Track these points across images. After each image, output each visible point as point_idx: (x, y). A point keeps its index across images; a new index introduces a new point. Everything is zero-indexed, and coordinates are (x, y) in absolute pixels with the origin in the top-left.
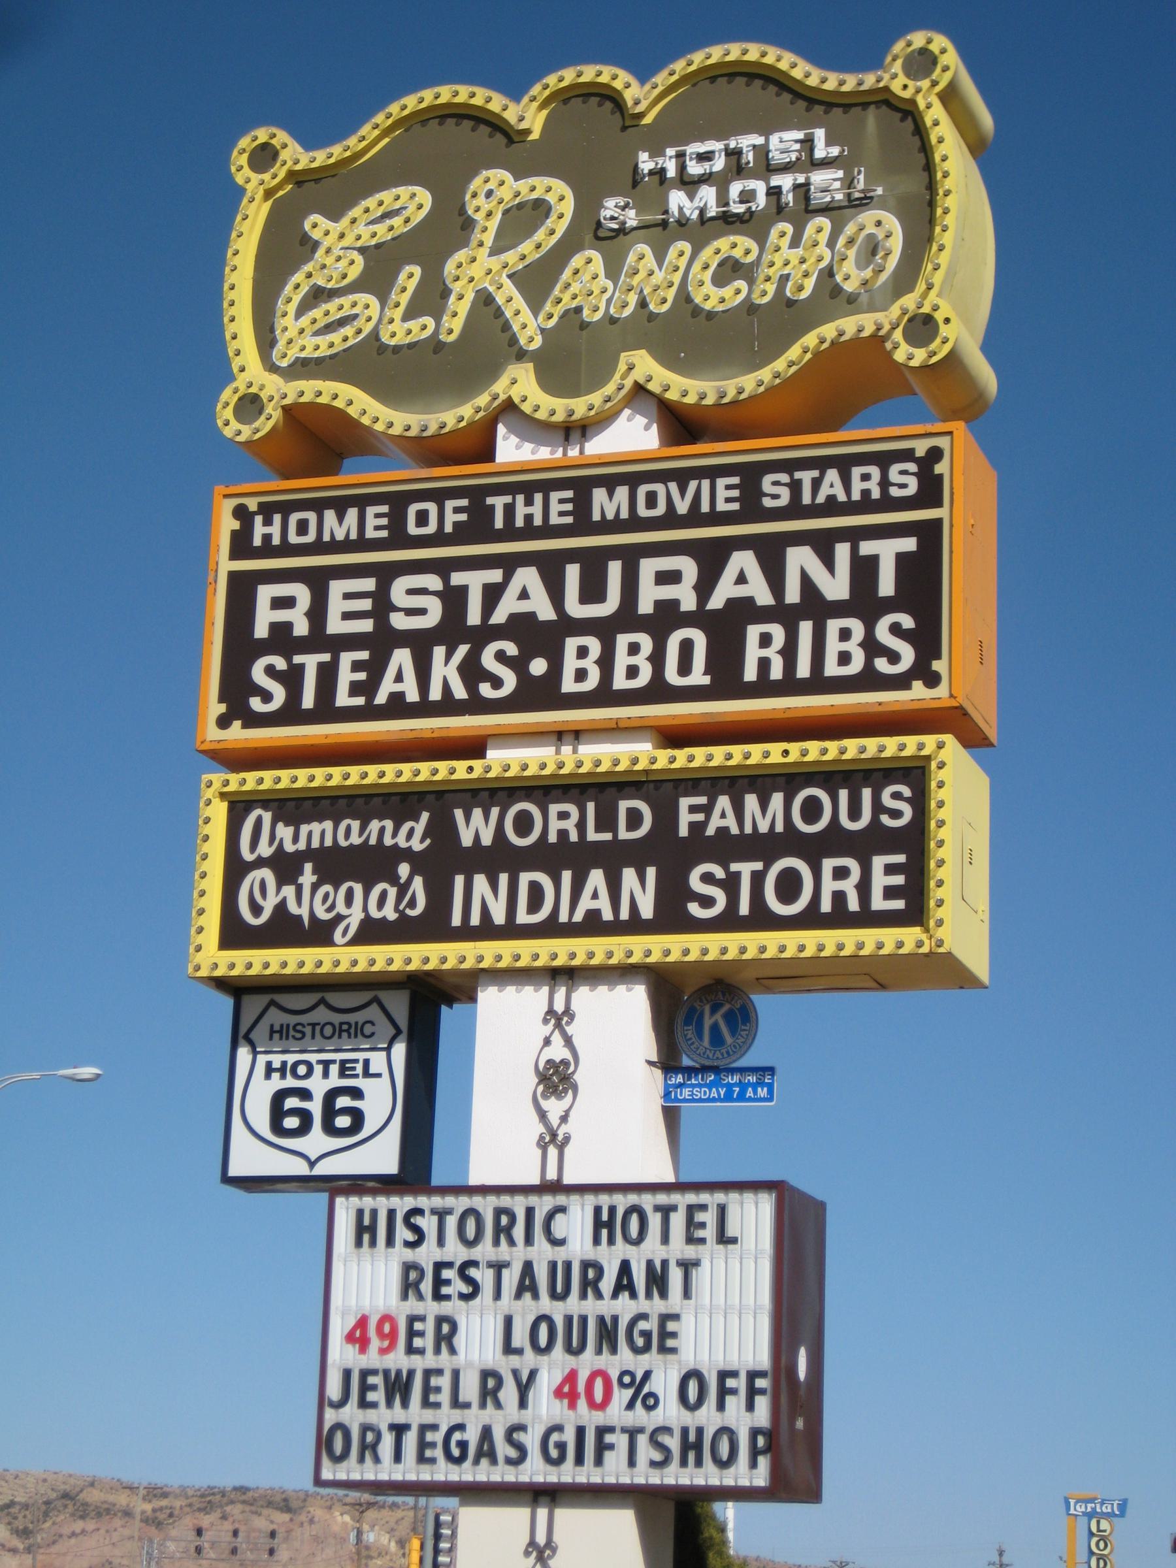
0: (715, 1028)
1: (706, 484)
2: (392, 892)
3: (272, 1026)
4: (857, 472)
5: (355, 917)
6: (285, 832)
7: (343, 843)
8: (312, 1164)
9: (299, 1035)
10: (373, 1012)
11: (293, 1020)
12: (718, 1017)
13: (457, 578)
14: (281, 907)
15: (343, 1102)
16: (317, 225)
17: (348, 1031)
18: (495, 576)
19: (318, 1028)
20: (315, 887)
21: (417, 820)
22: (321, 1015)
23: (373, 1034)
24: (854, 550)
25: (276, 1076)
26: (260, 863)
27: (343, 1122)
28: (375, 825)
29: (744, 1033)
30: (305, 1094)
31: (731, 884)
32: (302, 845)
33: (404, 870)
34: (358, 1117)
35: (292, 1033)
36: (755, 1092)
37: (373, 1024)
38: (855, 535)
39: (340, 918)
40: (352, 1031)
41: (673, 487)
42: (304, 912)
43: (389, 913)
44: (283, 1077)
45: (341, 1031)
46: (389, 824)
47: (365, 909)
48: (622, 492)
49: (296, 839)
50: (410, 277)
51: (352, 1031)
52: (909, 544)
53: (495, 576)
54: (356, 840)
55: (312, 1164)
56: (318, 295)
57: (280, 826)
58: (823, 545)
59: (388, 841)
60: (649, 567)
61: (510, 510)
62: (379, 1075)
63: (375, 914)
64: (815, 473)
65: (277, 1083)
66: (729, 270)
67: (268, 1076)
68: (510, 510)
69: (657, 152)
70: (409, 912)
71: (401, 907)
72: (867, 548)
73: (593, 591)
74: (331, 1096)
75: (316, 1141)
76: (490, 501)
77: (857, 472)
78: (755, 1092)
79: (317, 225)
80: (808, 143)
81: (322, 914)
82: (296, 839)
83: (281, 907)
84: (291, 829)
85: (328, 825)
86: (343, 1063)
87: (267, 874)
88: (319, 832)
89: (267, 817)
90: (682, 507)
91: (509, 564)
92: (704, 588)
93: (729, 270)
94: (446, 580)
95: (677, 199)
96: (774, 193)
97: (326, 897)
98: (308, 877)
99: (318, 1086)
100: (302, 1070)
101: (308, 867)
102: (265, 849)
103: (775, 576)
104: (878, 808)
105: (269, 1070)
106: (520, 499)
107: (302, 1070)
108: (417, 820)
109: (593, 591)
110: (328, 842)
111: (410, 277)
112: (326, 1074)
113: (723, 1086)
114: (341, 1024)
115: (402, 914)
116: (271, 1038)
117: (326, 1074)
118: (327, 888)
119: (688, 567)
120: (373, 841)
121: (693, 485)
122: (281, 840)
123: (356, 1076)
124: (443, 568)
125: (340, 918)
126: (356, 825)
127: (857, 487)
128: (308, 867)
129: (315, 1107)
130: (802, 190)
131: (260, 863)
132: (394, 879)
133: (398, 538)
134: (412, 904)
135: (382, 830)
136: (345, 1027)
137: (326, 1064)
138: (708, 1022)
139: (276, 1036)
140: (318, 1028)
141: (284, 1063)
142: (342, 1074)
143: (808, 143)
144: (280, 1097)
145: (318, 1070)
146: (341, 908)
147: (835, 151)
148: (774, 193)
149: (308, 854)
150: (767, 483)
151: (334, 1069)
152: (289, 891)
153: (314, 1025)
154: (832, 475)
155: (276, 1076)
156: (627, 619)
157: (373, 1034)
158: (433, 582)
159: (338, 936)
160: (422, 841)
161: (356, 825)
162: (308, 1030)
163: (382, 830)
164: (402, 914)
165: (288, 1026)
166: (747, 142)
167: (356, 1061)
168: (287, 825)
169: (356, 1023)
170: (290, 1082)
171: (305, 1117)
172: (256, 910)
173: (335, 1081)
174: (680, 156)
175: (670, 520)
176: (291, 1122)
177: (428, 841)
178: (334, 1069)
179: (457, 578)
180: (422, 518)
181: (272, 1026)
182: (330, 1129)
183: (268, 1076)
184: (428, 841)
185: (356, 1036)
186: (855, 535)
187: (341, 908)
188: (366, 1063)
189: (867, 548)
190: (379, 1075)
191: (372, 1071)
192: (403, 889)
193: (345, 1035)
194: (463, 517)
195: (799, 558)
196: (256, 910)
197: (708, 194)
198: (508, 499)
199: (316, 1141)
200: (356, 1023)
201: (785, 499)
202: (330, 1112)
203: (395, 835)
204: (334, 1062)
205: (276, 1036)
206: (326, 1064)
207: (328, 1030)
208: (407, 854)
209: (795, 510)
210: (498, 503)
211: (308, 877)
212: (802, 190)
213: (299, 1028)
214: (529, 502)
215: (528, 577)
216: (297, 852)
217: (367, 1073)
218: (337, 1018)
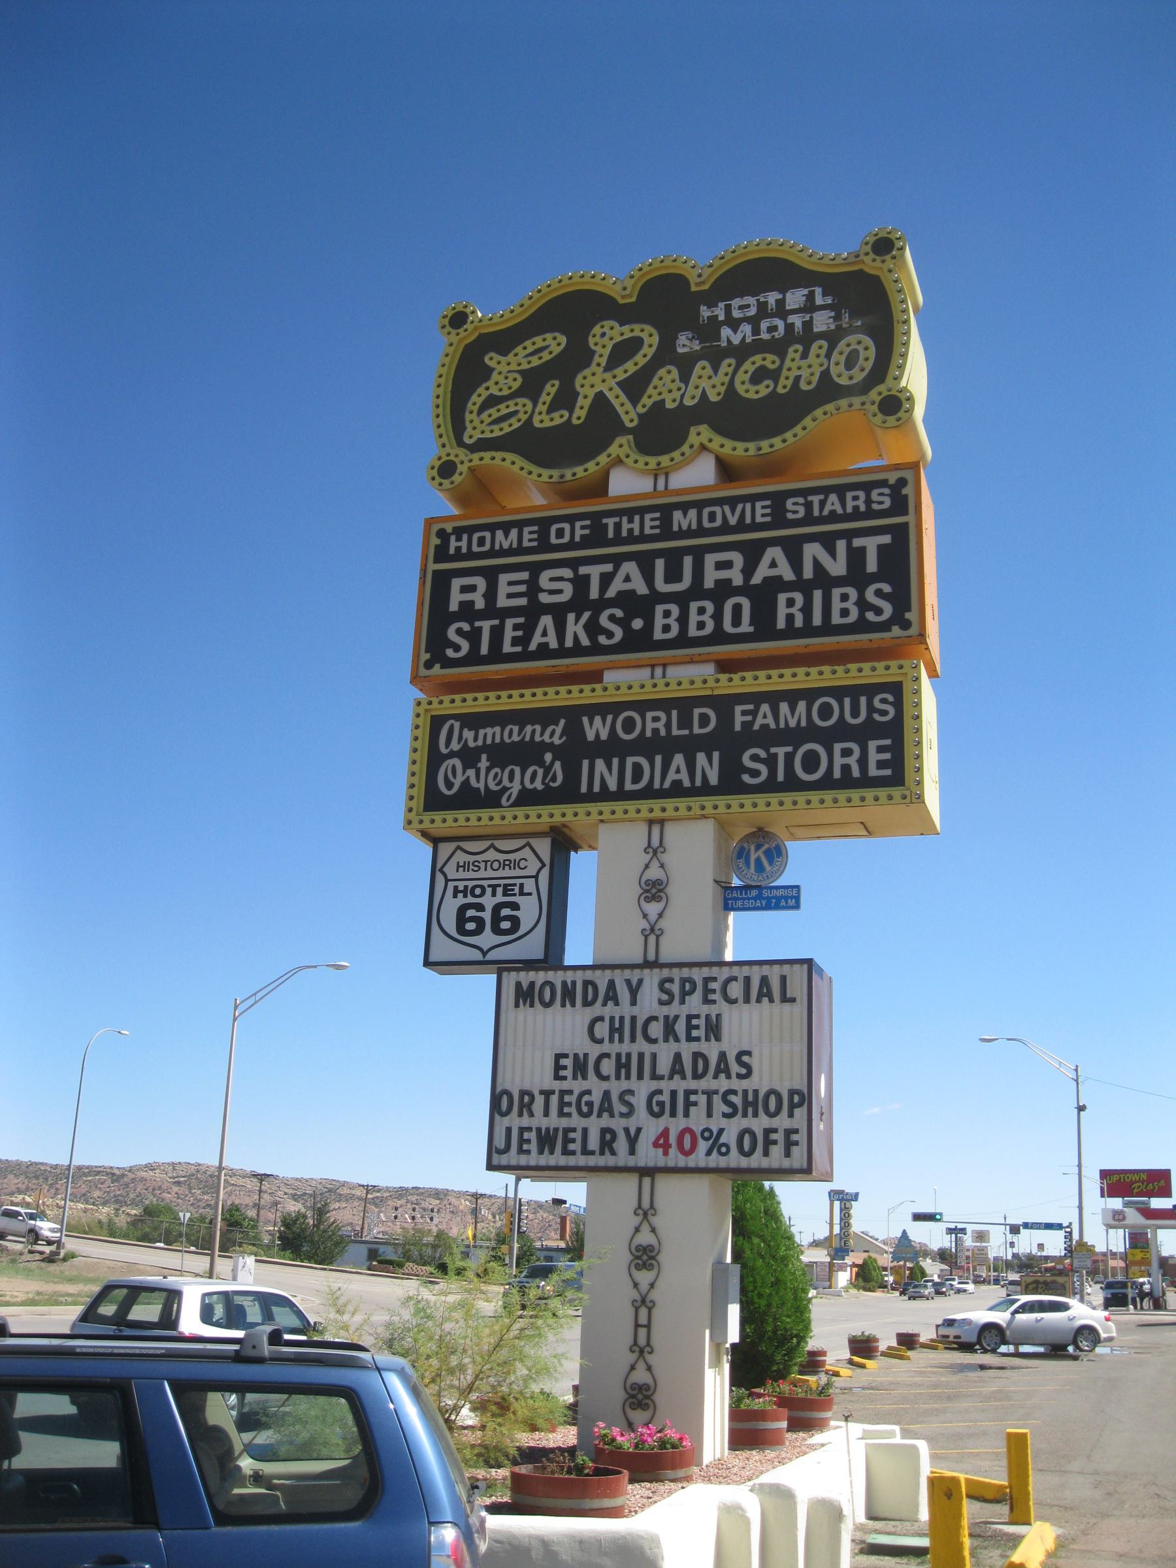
0: (758, 860)
2: (540, 772)
3: (458, 863)
5: (516, 788)
6: (468, 735)
8: (484, 953)
9: (476, 869)
10: (527, 852)
11: (472, 858)
12: (760, 853)
13: (583, 570)
14: (466, 783)
15: (505, 912)
16: (492, 359)
17: (464, 867)
18: (608, 568)
19: (489, 863)
20: (488, 770)
21: (557, 725)
22: (492, 855)
23: (526, 867)
24: (849, 544)
25: (460, 895)
26: (452, 755)
27: (505, 925)
28: (529, 728)
29: (778, 863)
30: (480, 907)
31: (771, 762)
32: (480, 743)
33: (548, 757)
34: (516, 922)
35: (471, 867)
36: (787, 903)
37: (526, 860)
39: (505, 789)
40: (512, 865)
41: (727, 508)
42: (481, 786)
43: (538, 784)
44: (465, 896)
45: (504, 865)
46: (538, 728)
50: (551, 388)
51: (512, 865)
53: (608, 568)
54: (516, 738)
55: (484, 953)
56: (492, 401)
57: (466, 731)
59: (538, 739)
60: (710, 559)
61: (618, 526)
62: (530, 894)
63: (528, 785)
64: (822, 497)
65: (461, 900)
66: (759, 376)
67: (455, 896)
68: (618, 526)
69: (712, 305)
70: (552, 784)
71: (547, 781)
72: (857, 542)
74: (497, 908)
75: (487, 938)
77: (849, 495)
78: (787, 903)
79: (492, 359)
81: (493, 787)
82: (476, 739)
83: (466, 783)
84: (473, 733)
85: (498, 729)
86: (506, 886)
88: (491, 734)
90: (733, 521)
91: (618, 560)
92: (748, 571)
94: (575, 571)
97: (496, 775)
98: (484, 763)
99: (489, 901)
100: (478, 891)
101: (484, 757)
102: (455, 746)
104: (871, 709)
105: (456, 891)
106: (625, 519)
107: (478, 891)
108: (557, 725)
110: (498, 740)
111: (551, 388)
112: (494, 894)
113: (764, 898)
114: (505, 861)
115: (547, 785)
116: (457, 871)
117: (494, 894)
118: (497, 770)
119: (737, 558)
120: (527, 739)
121: (740, 507)
122: (466, 739)
123: (515, 895)
124: (573, 564)
125: (505, 789)
126: (516, 729)
128: (484, 757)
129: (487, 915)
131: (452, 755)
132: (541, 763)
133: (544, 545)
134: (554, 779)
135: (534, 732)
136: (507, 863)
137: (494, 887)
138: (753, 857)
139: (461, 869)
140: (489, 863)
141: (466, 887)
142: (505, 894)
143: (811, 297)
144: (462, 910)
145: (489, 891)
146: (506, 782)
147: (829, 300)
148: (790, 327)
149: (485, 748)
151: (500, 890)
152: (471, 773)
153: (486, 862)
154: (833, 498)
155: (460, 895)
156: (697, 591)
157: (526, 867)
158: (567, 573)
159: (504, 801)
160: (560, 739)
161: (516, 729)
162: (482, 865)
163: (534, 732)
164: (547, 785)
165: (469, 862)
166: (772, 298)
167: (515, 885)
169: (515, 860)
170: (470, 900)
171: (480, 922)
172: (449, 785)
173: (500, 898)
174: (728, 309)
175: (725, 529)
176: (471, 926)
177: (564, 738)
178: (500, 890)
179: (583, 570)
180: (560, 533)
181: (458, 863)
182: (497, 930)
183: (455, 896)
184: (564, 738)
185: (514, 869)
186: (849, 535)
187: (506, 782)
188: (522, 885)
189: (857, 542)
190: (530, 894)
191: (525, 891)
193: (507, 867)
194: (587, 532)
196: (449, 785)
197: (746, 329)
198: (617, 519)
199: (487, 938)
200: (515, 860)
201: (801, 513)
202: (496, 918)
204: (499, 885)
205: (461, 869)
206: (494, 887)
207: (496, 865)
208: (550, 747)
209: (809, 520)
210: (610, 522)
211: (484, 763)
212: (808, 325)
213: (476, 864)
214: (631, 521)
215: (630, 568)
216: (477, 747)
217: (522, 893)
218: (501, 857)
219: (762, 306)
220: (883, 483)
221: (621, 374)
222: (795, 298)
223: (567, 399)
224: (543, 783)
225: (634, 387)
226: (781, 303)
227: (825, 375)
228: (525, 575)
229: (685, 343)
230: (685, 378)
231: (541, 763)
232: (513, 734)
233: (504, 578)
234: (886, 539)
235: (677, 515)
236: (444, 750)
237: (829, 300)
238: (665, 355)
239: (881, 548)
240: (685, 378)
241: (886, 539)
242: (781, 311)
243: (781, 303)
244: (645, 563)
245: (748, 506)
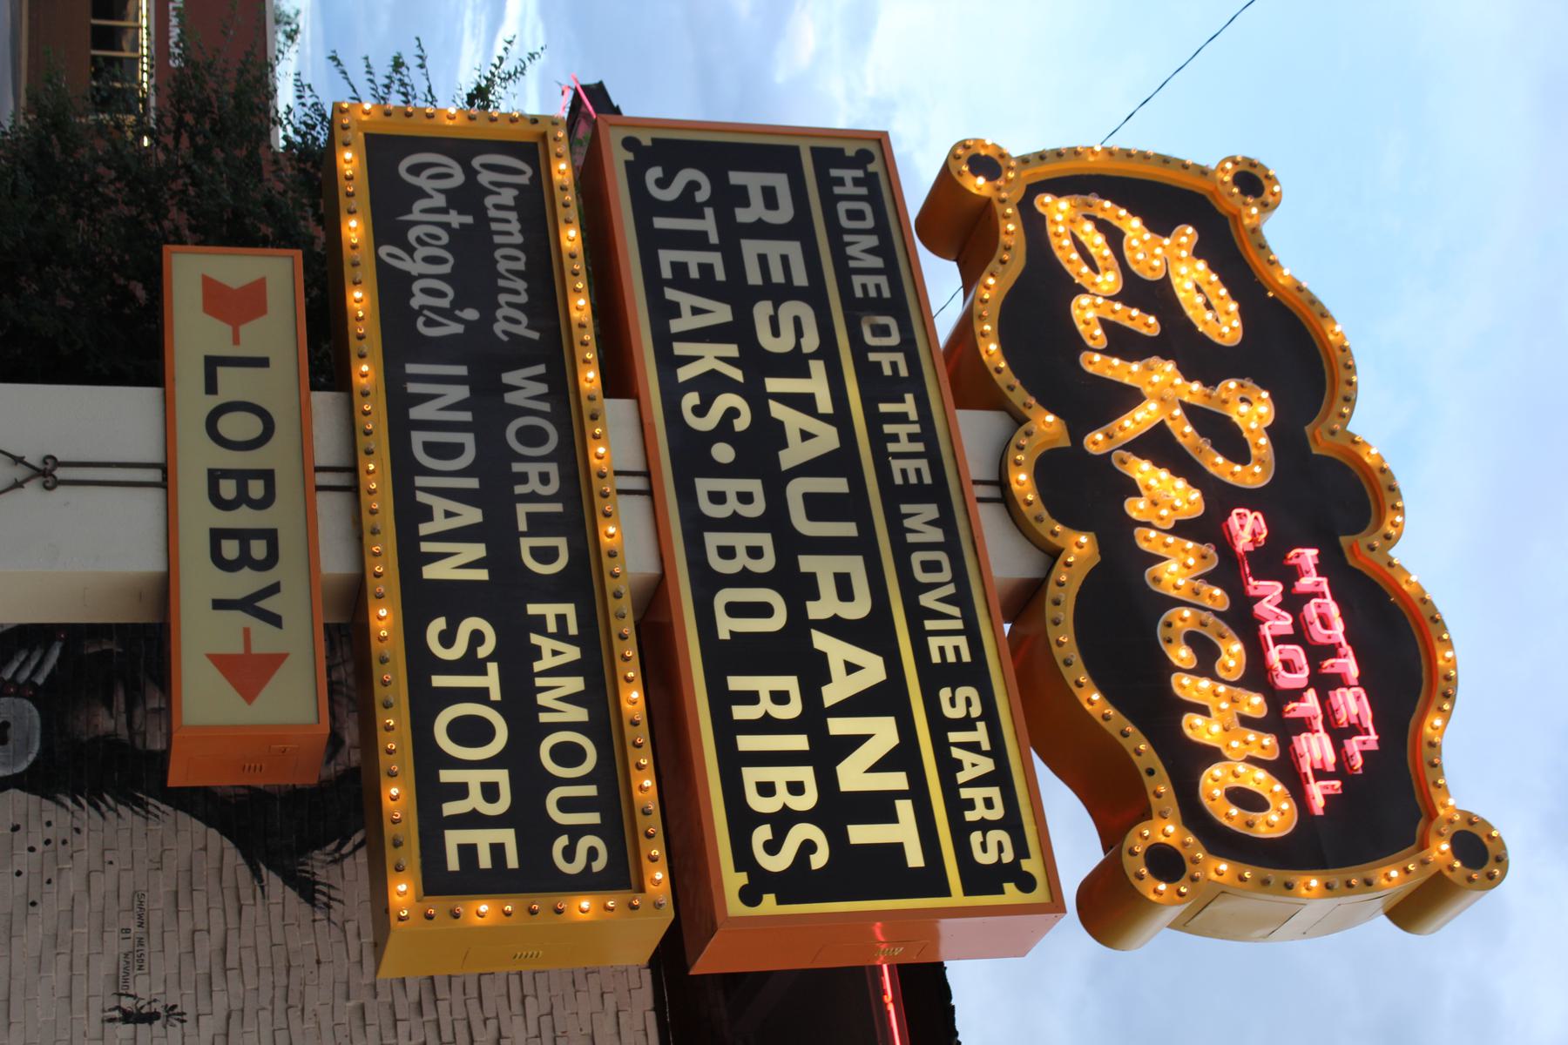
1: (958, 625)
2: (444, 303)
4: (994, 793)
6: (508, 196)
7: (498, 254)
16: (1187, 234)
20: (446, 226)
21: (529, 327)
24: (901, 795)
33: (471, 314)
38: (918, 792)
41: (950, 590)
42: (416, 216)
47: (422, 276)
48: (936, 535)
49: (498, 207)
50: (1149, 325)
52: (915, 858)
54: (503, 266)
56: (1114, 237)
57: (515, 192)
58: (903, 757)
61: (902, 418)
63: (417, 286)
68: (902, 418)
70: (421, 320)
71: (426, 312)
72: (905, 808)
73: (818, 506)
76: (909, 397)
79: (1187, 234)
80: (1356, 729)
83: (421, 194)
84: (511, 203)
85: (518, 239)
87: (458, 178)
89: (524, 180)
90: (927, 600)
93: (1207, 655)
94: (815, 355)
95: (1273, 589)
96: (1297, 695)
102: (485, 178)
103: (853, 706)
104: (576, 832)
108: (529, 327)
109: (818, 506)
110: (498, 239)
111: (1149, 325)
115: (420, 312)
118: (445, 239)
119: (859, 609)
120: (501, 283)
121: (954, 611)
122: (499, 194)
124: (828, 352)
125: (410, 250)
126: (520, 266)
127: (977, 794)
130: (1304, 725)
132: (458, 303)
134: (430, 323)
143: (1356, 729)
146: (422, 252)
148: (1297, 695)
150: (965, 692)
152: (440, 201)
154: (987, 765)
160: (505, 332)
161: (520, 266)
166: (1349, 665)
168: (515, 198)
172: (416, 170)
177: (505, 338)
180: (883, 331)
184: (505, 338)
186: (918, 792)
189: (905, 808)
192: (448, 314)
194: (887, 371)
195: (883, 733)
196: (416, 170)
197: (1285, 623)
198: (913, 416)
203: (510, 304)
208: (488, 318)
209: (940, 726)
210: (909, 406)
211: (455, 219)
214: (912, 438)
219: (1332, 650)
220: (1021, 850)
221: (1185, 432)
222: (1352, 703)
223: (1122, 343)
224: (423, 307)
225: (1157, 444)
226: (1339, 681)
227: (1212, 755)
228: (800, 279)
229: (1247, 528)
230: (1183, 529)
231: (458, 303)
232: (509, 261)
233: (794, 249)
234: (915, 858)
235: (931, 511)
236: (476, 162)
237: (1358, 762)
238: (1221, 498)
239: (897, 849)
240: (1183, 529)
241: (915, 858)
242: (1325, 684)
243: (1339, 681)
244: (840, 461)
245: (958, 625)
